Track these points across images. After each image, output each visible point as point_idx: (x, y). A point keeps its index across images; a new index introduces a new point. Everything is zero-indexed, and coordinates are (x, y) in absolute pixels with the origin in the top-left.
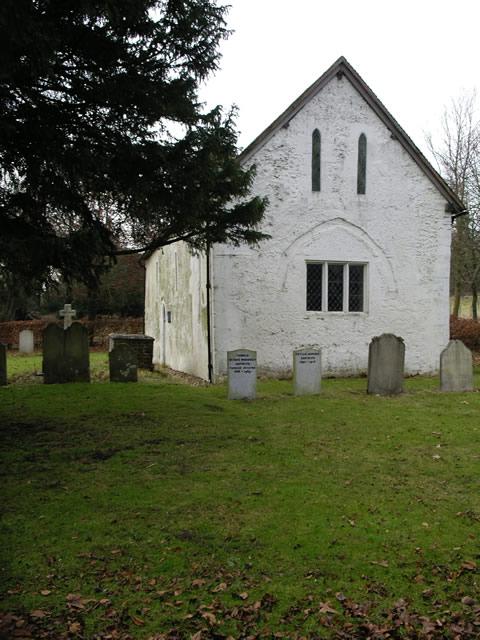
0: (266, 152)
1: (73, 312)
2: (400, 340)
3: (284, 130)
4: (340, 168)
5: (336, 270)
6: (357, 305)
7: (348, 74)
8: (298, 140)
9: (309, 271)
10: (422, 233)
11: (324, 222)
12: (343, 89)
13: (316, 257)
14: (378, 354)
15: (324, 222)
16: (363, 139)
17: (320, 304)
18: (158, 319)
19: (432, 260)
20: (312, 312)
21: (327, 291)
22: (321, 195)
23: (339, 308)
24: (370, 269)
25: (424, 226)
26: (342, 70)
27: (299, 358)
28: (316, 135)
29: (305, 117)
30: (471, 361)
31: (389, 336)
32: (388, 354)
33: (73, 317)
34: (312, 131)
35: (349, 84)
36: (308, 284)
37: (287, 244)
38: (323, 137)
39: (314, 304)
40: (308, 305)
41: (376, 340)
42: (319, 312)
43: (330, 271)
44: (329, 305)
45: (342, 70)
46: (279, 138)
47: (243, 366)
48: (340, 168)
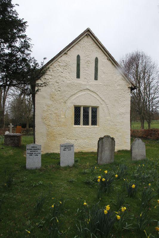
0: (58, 63)
1: (13, 126)
2: (113, 139)
3: (65, 55)
4: (87, 70)
5: (86, 109)
6: (94, 123)
7: (91, 35)
8: (70, 59)
9: (75, 109)
10: (119, 95)
11: (81, 90)
12: (87, 42)
13: (78, 104)
14: (102, 146)
15: (81, 90)
16: (97, 60)
17: (80, 123)
18: (87, 128)
19: (94, 104)
20: (76, 126)
21: (82, 120)
22: (80, 81)
23: (88, 124)
24: (100, 108)
25: (120, 93)
26: (88, 33)
27: (63, 148)
28: (78, 57)
29: (74, 50)
30: (145, 148)
31: (108, 137)
32: (107, 147)
33: (12, 128)
34: (77, 54)
35: (91, 39)
36: (75, 115)
37: (66, 99)
38: (81, 58)
39: (77, 122)
40: (75, 123)
41: (101, 139)
42: (95, 126)
43: (84, 110)
44: (92, 123)
45: (88, 33)
46: (64, 58)
47: (34, 153)
48: (87, 70)
